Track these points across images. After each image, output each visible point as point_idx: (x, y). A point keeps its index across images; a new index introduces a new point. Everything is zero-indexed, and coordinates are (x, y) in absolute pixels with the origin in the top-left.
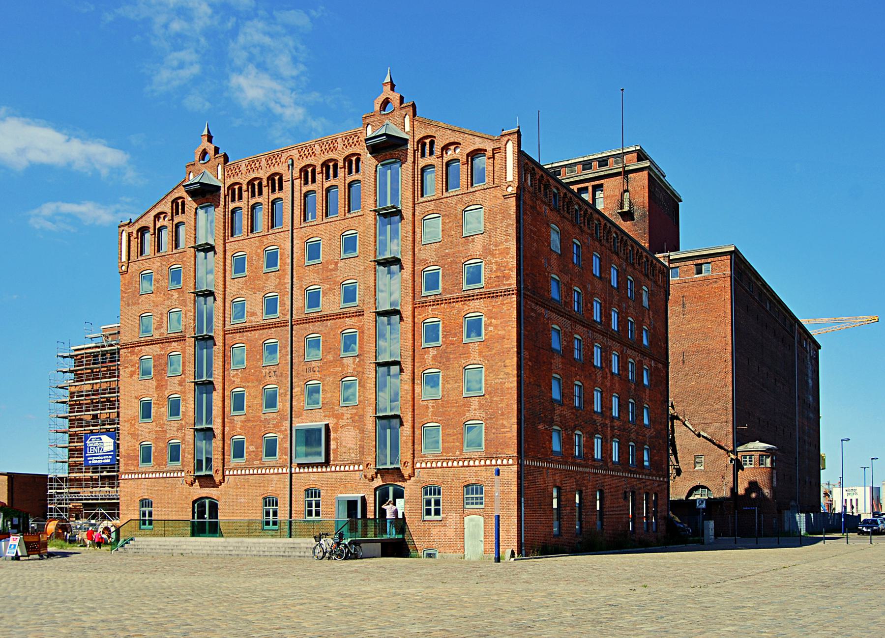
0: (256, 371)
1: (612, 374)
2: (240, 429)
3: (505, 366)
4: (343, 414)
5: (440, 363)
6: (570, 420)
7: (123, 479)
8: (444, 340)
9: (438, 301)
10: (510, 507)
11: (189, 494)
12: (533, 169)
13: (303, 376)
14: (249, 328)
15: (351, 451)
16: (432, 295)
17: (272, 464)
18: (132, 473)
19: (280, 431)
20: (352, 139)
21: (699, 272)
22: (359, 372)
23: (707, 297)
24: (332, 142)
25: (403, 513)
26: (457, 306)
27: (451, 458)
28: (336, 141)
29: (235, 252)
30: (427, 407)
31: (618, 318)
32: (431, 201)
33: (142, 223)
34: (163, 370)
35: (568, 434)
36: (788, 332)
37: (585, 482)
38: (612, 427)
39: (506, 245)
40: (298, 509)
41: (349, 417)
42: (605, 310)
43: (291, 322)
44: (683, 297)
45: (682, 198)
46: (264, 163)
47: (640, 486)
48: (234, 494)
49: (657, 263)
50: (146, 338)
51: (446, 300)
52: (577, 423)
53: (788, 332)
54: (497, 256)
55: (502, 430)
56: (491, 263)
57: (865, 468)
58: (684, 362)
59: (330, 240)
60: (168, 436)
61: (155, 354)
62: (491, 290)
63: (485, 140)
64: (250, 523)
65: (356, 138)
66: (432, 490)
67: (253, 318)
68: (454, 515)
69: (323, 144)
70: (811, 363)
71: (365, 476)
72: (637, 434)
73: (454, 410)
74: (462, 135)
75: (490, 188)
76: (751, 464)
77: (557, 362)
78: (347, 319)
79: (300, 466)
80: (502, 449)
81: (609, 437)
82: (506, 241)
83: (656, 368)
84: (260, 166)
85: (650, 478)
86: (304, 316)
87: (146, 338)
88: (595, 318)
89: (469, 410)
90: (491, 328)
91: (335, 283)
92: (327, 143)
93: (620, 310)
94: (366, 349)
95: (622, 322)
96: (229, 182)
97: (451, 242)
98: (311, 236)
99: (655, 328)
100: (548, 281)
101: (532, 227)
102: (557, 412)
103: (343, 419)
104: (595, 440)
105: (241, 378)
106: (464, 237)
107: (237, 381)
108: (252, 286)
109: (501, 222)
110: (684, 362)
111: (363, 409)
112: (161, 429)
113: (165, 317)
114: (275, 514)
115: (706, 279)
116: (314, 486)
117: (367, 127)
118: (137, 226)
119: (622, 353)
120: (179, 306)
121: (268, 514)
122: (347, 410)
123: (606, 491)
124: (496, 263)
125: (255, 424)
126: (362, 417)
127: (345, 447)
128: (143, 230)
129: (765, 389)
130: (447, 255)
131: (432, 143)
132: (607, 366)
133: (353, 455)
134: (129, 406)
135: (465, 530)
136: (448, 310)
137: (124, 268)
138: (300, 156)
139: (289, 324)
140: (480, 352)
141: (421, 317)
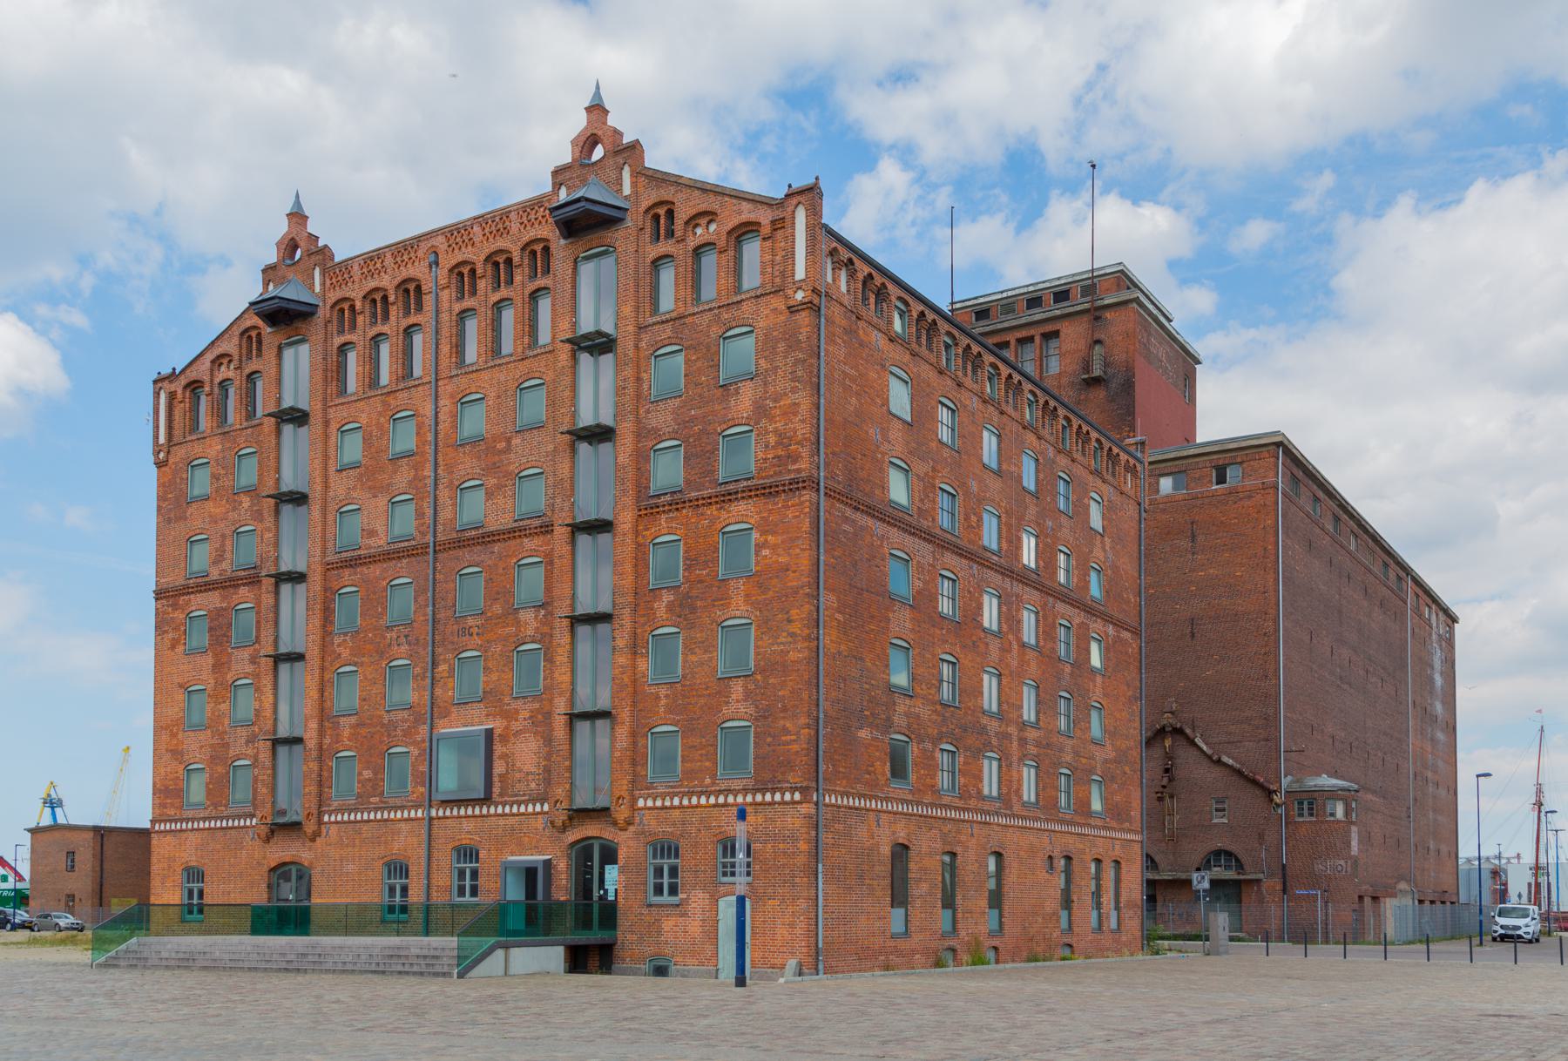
0: (375, 636)
1: (1023, 645)
2: (349, 740)
3: (789, 621)
4: (517, 712)
5: (680, 617)
6: (929, 724)
7: (157, 832)
8: (686, 574)
9: (677, 504)
10: (797, 880)
11: (264, 858)
12: (850, 261)
13: (453, 643)
14: (365, 558)
15: (530, 777)
16: (666, 494)
17: (399, 802)
18: (171, 821)
19: (415, 743)
20: (534, 211)
21: (1221, 479)
22: (544, 635)
23: (1234, 524)
24: (501, 219)
25: (616, 890)
26: (709, 512)
27: (696, 790)
28: (507, 217)
29: (343, 422)
30: (658, 698)
31: (1037, 545)
32: (667, 321)
33: (192, 375)
34: (224, 635)
35: (924, 751)
36: (1392, 590)
37: (963, 838)
38: (1023, 741)
39: (793, 398)
40: (441, 883)
41: (528, 715)
42: (1009, 531)
43: (435, 546)
44: (1192, 523)
45: (1201, 358)
46: (389, 261)
47: (1081, 846)
48: (337, 857)
49: (1122, 454)
50: (198, 580)
51: (691, 501)
52: (944, 730)
53: (1392, 590)
54: (778, 418)
55: (783, 738)
56: (767, 432)
57: (1557, 831)
58: (1193, 635)
59: (499, 397)
60: (231, 753)
61: (211, 607)
62: (766, 481)
63: (758, 205)
64: (363, 908)
65: (542, 209)
66: (667, 848)
67: (371, 542)
68: (701, 895)
69: (487, 223)
70: (1441, 646)
71: (552, 823)
72: (1076, 754)
73: (702, 701)
74: (719, 198)
75: (766, 294)
76: (1311, 815)
77: (901, 621)
78: (526, 540)
79: (445, 805)
80: (783, 773)
81: (1015, 758)
82: (794, 390)
83: (1118, 639)
84: (382, 267)
85: (1103, 833)
86: (455, 535)
87: (198, 580)
88: (986, 543)
89: (728, 702)
90: (766, 552)
91: (508, 474)
92: (493, 221)
93: (1041, 531)
94: (557, 592)
95: (1046, 554)
96: (333, 296)
97: (700, 395)
98: (468, 392)
99: (1115, 568)
100: (881, 470)
101: (847, 369)
102: (901, 709)
103: (517, 720)
104: (986, 762)
105: (352, 649)
106: (721, 386)
107: (345, 653)
108: (370, 483)
109: (786, 357)
110: (1193, 635)
111: (551, 701)
112: (219, 741)
113: (228, 542)
114: (405, 890)
115: (1233, 492)
116: (468, 842)
117: (559, 189)
118: (183, 381)
119: (1043, 609)
120: (251, 522)
121: (392, 890)
122: (525, 703)
123: (1009, 857)
124: (776, 431)
125: (372, 730)
126: (548, 715)
127: (520, 771)
128: (194, 386)
129: (1345, 686)
130: (693, 419)
131: (670, 214)
132: (1010, 628)
133: (533, 785)
134: (169, 700)
135: (720, 923)
136: (693, 520)
137: (162, 455)
138: (449, 246)
139: (431, 550)
140: (747, 596)
141: (648, 533)
